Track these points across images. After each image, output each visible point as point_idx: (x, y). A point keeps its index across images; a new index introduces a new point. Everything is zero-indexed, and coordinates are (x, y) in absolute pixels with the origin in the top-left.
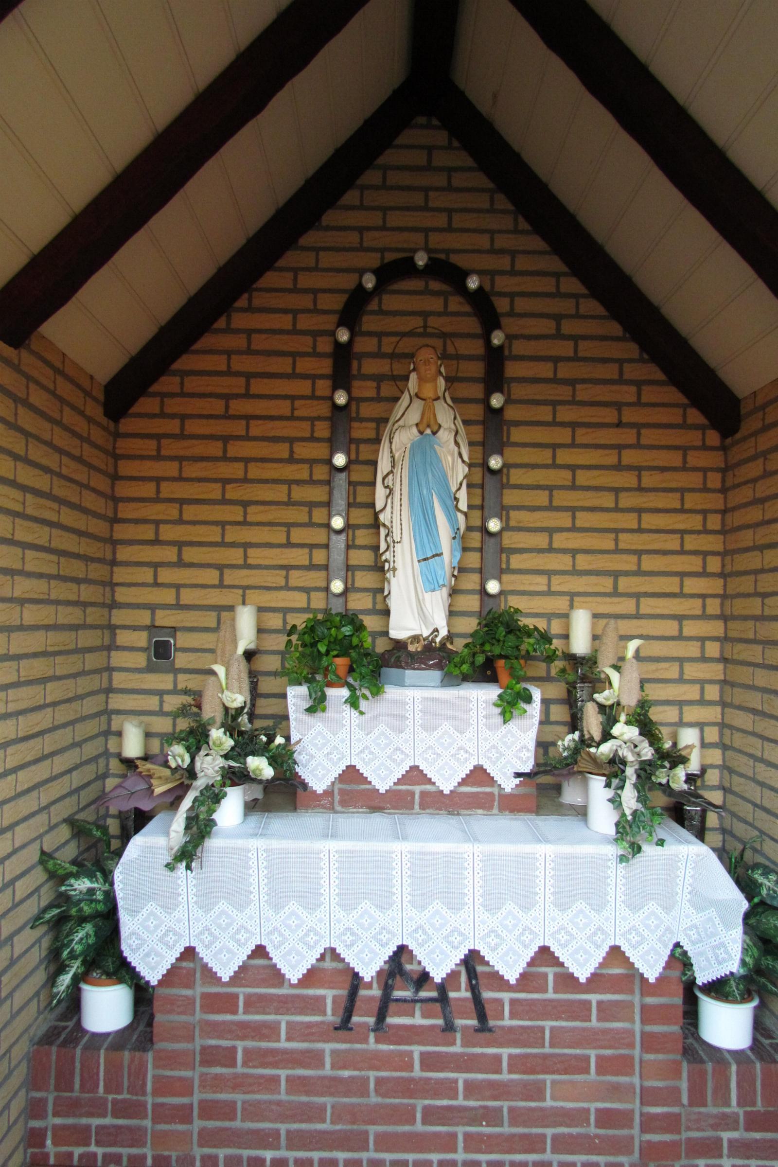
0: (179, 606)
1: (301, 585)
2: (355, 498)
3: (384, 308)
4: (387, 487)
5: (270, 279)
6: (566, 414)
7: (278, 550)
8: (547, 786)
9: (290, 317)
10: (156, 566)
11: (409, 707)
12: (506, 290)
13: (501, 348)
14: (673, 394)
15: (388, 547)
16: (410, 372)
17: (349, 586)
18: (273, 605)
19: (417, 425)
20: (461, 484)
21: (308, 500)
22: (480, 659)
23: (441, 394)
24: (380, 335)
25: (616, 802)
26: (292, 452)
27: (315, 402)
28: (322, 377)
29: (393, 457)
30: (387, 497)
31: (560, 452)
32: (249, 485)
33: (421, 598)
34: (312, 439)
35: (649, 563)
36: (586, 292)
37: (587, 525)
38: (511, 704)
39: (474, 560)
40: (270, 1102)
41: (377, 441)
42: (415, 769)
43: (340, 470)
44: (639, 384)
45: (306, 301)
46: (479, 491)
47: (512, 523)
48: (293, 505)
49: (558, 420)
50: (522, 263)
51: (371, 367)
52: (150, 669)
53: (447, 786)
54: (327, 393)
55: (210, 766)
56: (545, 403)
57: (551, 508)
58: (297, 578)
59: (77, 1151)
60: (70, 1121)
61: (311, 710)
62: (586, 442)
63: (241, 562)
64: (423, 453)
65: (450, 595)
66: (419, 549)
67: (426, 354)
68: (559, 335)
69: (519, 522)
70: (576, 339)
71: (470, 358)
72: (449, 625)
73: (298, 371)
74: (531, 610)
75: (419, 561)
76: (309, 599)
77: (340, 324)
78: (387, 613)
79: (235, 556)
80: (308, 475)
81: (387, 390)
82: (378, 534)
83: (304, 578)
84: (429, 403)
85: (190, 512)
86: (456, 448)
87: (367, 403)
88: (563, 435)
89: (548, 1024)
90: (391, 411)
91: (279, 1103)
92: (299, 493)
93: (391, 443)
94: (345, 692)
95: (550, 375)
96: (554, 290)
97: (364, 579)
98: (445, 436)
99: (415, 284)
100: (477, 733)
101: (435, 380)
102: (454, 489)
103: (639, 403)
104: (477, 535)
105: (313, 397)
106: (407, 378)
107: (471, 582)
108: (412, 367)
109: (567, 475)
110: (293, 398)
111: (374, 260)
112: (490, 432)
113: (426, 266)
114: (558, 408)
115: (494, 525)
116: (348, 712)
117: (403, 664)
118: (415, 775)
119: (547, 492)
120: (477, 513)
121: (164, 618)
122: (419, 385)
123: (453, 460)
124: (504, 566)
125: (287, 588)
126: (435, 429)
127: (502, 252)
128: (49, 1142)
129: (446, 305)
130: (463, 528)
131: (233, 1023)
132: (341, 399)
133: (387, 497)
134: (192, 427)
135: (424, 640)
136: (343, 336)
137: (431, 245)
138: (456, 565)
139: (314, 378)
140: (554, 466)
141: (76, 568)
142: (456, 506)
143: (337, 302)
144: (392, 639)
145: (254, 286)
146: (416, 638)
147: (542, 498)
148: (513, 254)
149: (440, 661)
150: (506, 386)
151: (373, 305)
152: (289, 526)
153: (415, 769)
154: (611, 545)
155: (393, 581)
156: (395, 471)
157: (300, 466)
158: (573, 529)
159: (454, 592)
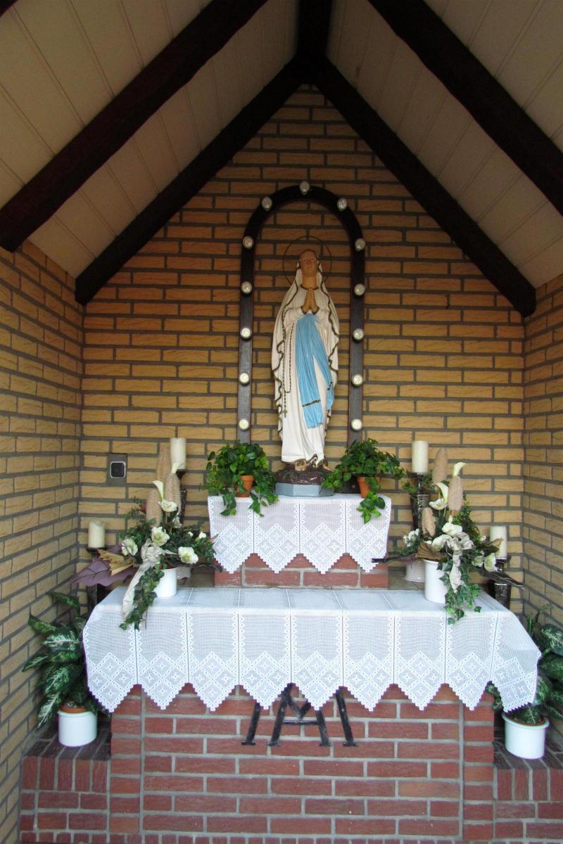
0: (129, 438)
1: (218, 423)
2: (257, 360)
4: (280, 352)
5: (195, 202)
6: (409, 300)
8: (396, 568)
10: (113, 409)
13: (362, 251)
14: (487, 285)
17: (253, 423)
19: (302, 307)
20: (333, 350)
21: (223, 361)
22: (347, 477)
23: (319, 286)
24: (275, 242)
25: (446, 580)
26: (211, 327)
27: (228, 291)
28: (233, 273)
29: (284, 330)
30: (280, 360)
34: (226, 317)
35: (470, 407)
38: (369, 509)
39: (343, 405)
40: (196, 797)
41: (273, 319)
42: (300, 556)
43: (246, 340)
44: (462, 278)
45: (221, 218)
46: (346, 355)
47: (371, 379)
49: (404, 304)
51: (268, 265)
52: (109, 484)
53: (323, 569)
55: (152, 554)
57: (398, 367)
58: (215, 418)
59: (56, 832)
61: (225, 514)
64: (306, 327)
65: (326, 430)
67: (308, 256)
68: (404, 243)
69: (376, 378)
70: (416, 245)
71: (340, 259)
73: (215, 268)
74: (384, 441)
76: (224, 433)
77: (246, 234)
78: (279, 443)
79: (170, 402)
81: (280, 282)
82: (274, 386)
84: (310, 291)
85: (138, 370)
88: (407, 315)
89: (397, 740)
90: (283, 297)
91: (202, 798)
92: (216, 357)
93: (283, 320)
94: (250, 501)
96: (401, 210)
97: (263, 419)
98: (322, 315)
99: (301, 206)
100: (345, 530)
102: (328, 354)
104: (345, 387)
105: (227, 287)
106: (294, 273)
107: (341, 421)
108: (298, 265)
109: (410, 343)
110: (212, 288)
112: (354, 312)
113: (308, 192)
115: (357, 380)
116: (252, 515)
117: (292, 480)
118: (300, 560)
120: (345, 371)
121: (119, 447)
122: (303, 279)
123: (328, 333)
125: (208, 425)
126: (315, 310)
127: (363, 182)
128: (35, 826)
129: (323, 220)
130: (335, 381)
131: (168, 739)
132: (247, 288)
133: (280, 360)
134: (139, 309)
135: (307, 463)
136: (249, 243)
137: (312, 177)
139: (227, 273)
140: (401, 337)
142: (330, 366)
143: (244, 219)
146: (301, 462)
147: (392, 360)
148: (371, 184)
149: (319, 478)
151: (270, 221)
152: (209, 380)
153: (300, 556)
154: (442, 395)
155: (285, 420)
158: (415, 382)
159: (328, 428)
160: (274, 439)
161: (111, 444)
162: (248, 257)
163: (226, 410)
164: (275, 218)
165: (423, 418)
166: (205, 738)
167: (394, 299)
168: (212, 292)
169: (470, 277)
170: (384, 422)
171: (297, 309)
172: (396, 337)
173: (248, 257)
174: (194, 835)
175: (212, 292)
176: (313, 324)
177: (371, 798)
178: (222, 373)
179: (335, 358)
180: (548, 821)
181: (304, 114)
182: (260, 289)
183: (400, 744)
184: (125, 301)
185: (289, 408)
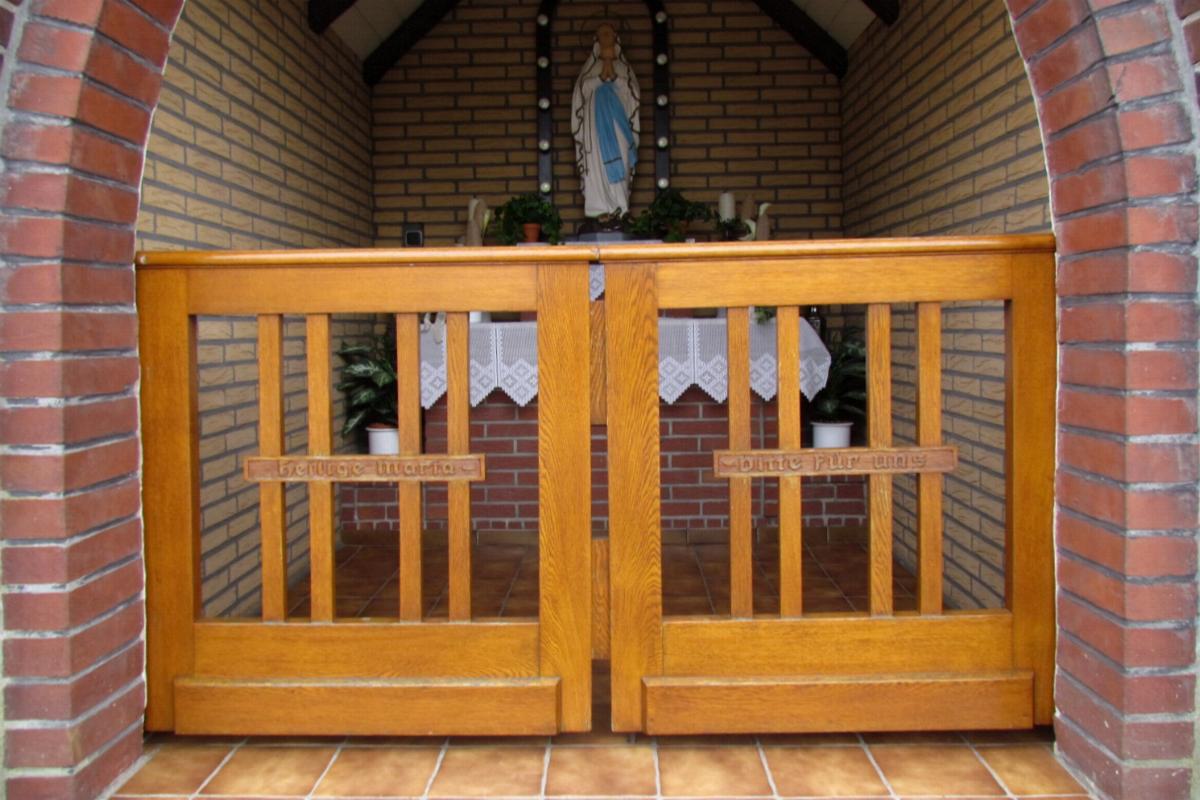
4: (579, 117)
13: (665, 24)
14: (798, 50)
16: (594, 42)
17: (555, 188)
20: (634, 113)
24: (571, 20)
40: (508, 490)
41: (571, 91)
43: (545, 152)
44: (773, 45)
51: (564, 41)
59: (375, 522)
60: (369, 504)
63: (472, 177)
71: (642, 32)
81: (578, 56)
89: (699, 437)
91: (513, 490)
92: (513, 129)
101: (613, 46)
102: (629, 115)
103: (773, 57)
105: (522, 63)
106: (591, 48)
121: (413, 217)
123: (628, 98)
128: (356, 517)
131: (480, 442)
132: (543, 63)
134: (431, 88)
136: (543, 21)
139: (522, 51)
141: (352, 177)
146: (605, 215)
154: (755, 155)
155: (587, 179)
161: (405, 215)
163: (526, 178)
166: (515, 440)
169: (781, 43)
171: (595, 77)
174: (507, 521)
176: (612, 91)
177: (676, 485)
180: (847, 500)
181: (449, 44)
182: (559, 64)
183: (703, 440)
184: (415, 81)
185: (590, 167)
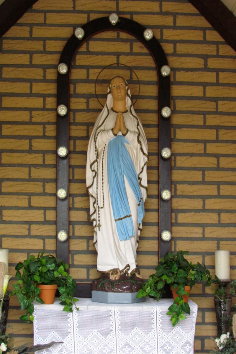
1: (39, 234)
2: (73, 176)
3: (91, 50)
4: (93, 171)
5: (14, 31)
6: (212, 120)
7: (23, 211)
9: (28, 56)
11: (112, 318)
12: (171, 38)
13: (168, 77)
15: (95, 211)
16: (108, 94)
17: (71, 234)
18: (21, 247)
19: (112, 130)
20: (143, 169)
21: (42, 177)
22: (160, 286)
23: (128, 109)
24: (88, 68)
26: (31, 146)
27: (45, 113)
28: (50, 95)
29: (97, 151)
30: (94, 177)
31: (208, 146)
32: (4, 168)
33: (117, 244)
34: (44, 137)
36: (223, 40)
37: (227, 194)
38: (177, 314)
39: (153, 217)
41: (87, 138)
43: (64, 158)
45: (38, 45)
46: (155, 172)
47: (178, 193)
48: (32, 181)
49: (207, 124)
50: (181, 21)
51: (82, 89)
54: (54, 106)
56: (199, 113)
57: (204, 182)
58: (36, 230)
62: (226, 139)
65: (138, 242)
66: (116, 212)
67: (117, 82)
68: (206, 69)
69: (183, 192)
70: (217, 71)
72: (136, 261)
73: (33, 92)
74: (192, 251)
75: (116, 220)
76: (44, 243)
77: (61, 61)
80: (42, 161)
81: (94, 104)
82: (89, 200)
83: (41, 230)
84: (120, 114)
86: (139, 145)
87: (81, 113)
90: (96, 118)
93: (95, 141)
95: (201, 94)
96: (202, 39)
97: (80, 231)
98: (131, 137)
99: (111, 34)
101: (124, 99)
102: (138, 172)
104: (155, 201)
105: (44, 109)
106: (105, 96)
107: (152, 231)
108: (109, 91)
109: (214, 160)
110: (31, 110)
111: (83, 19)
113: (118, 23)
114: (207, 116)
115: (166, 195)
117: (106, 289)
119: (201, 172)
120: (155, 186)
122: (114, 103)
123: (137, 152)
124: (173, 221)
125: (29, 236)
126: (125, 132)
127: (167, 13)
129: (131, 48)
130: (145, 197)
133: (94, 177)
135: (120, 272)
136: (63, 69)
137: (121, 9)
138: (141, 223)
139: (44, 96)
142: (140, 183)
143: (58, 46)
144: (98, 271)
145: (4, 36)
146: (115, 271)
148: (175, 15)
149: (131, 286)
150: (172, 102)
151: (83, 48)
152: (30, 195)
155: (99, 233)
156: (98, 160)
157: (37, 155)
158: (219, 196)
159: (140, 239)
160: (91, 248)
162: (63, 84)
163: (46, 222)
164: (88, 46)
165: (226, 228)
167: (198, 120)
168: (31, 114)
170: (191, 233)
171: (108, 131)
172: (200, 155)
173: (63, 84)
175: (31, 114)
178: (42, 188)
179: (144, 176)
185: (102, 223)
